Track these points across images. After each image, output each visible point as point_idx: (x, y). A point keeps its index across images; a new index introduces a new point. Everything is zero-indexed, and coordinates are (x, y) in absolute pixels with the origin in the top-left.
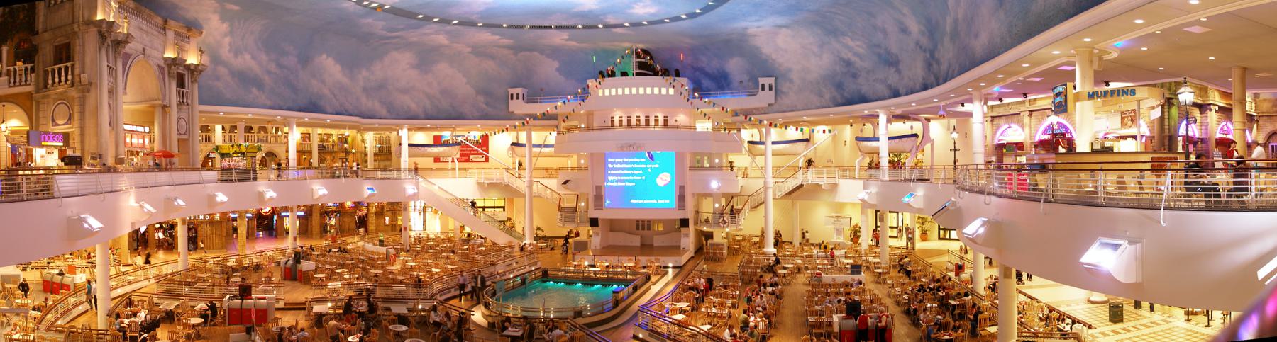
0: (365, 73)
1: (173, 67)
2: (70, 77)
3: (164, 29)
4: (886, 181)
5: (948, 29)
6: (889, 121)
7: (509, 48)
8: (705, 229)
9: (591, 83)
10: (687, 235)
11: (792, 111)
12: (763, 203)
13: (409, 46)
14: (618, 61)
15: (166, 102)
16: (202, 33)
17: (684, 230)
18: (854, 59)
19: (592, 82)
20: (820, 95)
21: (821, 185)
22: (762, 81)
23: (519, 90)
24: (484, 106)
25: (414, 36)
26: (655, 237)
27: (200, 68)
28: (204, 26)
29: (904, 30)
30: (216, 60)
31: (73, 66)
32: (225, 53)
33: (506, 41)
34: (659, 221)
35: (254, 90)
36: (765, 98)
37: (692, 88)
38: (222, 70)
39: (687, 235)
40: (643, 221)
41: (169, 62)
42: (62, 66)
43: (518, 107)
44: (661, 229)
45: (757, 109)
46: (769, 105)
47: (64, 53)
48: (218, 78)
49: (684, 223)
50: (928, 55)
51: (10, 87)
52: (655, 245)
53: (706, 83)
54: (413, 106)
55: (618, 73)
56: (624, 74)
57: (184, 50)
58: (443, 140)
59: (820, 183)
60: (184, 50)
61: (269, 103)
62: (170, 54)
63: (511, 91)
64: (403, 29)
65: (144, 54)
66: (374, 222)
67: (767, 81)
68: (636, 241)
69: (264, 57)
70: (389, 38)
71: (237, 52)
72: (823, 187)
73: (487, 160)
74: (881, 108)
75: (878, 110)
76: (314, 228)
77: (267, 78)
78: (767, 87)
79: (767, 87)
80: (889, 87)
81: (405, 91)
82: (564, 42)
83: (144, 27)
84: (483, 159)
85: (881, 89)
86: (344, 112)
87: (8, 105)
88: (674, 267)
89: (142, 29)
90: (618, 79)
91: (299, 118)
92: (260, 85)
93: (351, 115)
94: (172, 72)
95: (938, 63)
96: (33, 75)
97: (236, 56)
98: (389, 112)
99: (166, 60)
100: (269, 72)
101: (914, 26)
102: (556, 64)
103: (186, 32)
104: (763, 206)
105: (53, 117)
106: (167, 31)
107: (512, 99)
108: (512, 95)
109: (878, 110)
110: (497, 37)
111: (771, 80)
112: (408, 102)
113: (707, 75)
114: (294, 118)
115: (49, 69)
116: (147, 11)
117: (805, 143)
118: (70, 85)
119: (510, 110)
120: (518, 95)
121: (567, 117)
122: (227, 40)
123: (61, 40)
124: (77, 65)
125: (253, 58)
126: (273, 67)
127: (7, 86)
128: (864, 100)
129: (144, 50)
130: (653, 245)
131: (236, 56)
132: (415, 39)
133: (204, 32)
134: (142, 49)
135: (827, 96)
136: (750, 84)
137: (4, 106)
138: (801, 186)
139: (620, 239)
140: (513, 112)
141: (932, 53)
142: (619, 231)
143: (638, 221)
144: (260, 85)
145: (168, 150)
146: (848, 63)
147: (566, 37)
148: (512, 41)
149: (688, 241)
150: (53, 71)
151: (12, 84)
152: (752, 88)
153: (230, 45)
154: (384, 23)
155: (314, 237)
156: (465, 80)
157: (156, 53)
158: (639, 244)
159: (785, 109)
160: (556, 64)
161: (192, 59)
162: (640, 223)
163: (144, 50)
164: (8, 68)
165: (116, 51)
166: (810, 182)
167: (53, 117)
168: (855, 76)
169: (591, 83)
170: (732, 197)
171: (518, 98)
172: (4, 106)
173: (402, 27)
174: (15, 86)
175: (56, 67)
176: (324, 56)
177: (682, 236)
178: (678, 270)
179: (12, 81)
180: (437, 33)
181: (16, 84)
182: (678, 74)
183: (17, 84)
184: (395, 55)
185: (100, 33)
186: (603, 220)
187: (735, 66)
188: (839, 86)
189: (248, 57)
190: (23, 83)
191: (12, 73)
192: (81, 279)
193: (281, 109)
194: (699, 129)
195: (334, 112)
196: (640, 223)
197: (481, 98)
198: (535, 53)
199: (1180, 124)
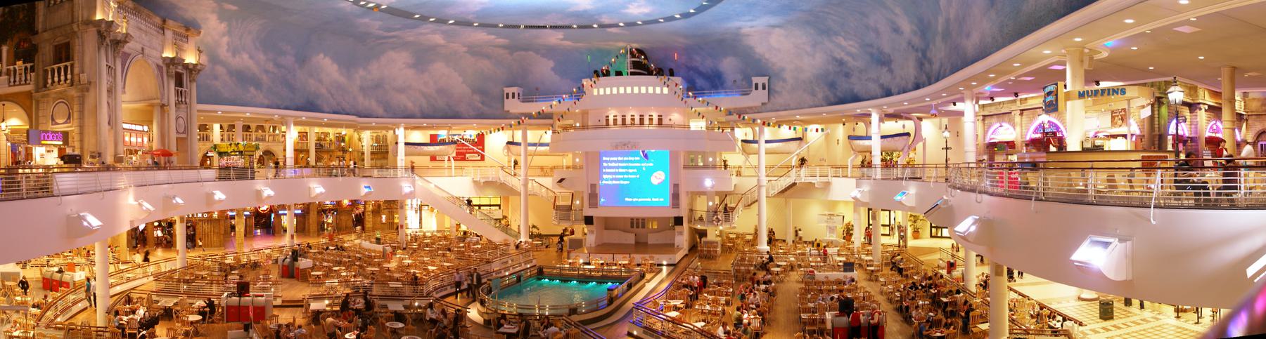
0: (361, 72)
1: (171, 67)
2: (69, 76)
3: (163, 29)
4: (879, 179)
5: (940, 29)
6: (881, 120)
7: (504, 47)
8: (699, 227)
9: (586, 82)
10: (681, 233)
11: (786, 110)
12: (757, 201)
13: (405, 45)
14: (613, 60)
15: (165, 101)
16: (200, 32)
17: (678, 228)
18: (846, 58)
19: (587, 82)
20: (813, 94)
21: (814, 184)
22: (755, 80)
23: (515, 90)
24: (480, 105)
25: (410, 36)
26: (649, 235)
27: (198, 67)
28: (202, 26)
29: (896, 30)
30: (214, 59)
31: (72, 66)
32: (223, 52)
33: (501, 41)
34: (653, 219)
35: (252, 89)
36: (758, 97)
37: (686, 87)
38: (220, 70)
39: (681, 233)
40: (638, 219)
41: (168, 61)
42: (62, 65)
43: (514, 106)
44: (655, 227)
45: (751, 108)
46: (763, 104)
47: (64, 53)
48: (216, 78)
49: (678, 221)
50: (920, 55)
51: (10, 86)
52: (649, 243)
53: (700, 82)
54: (410, 105)
55: (612, 72)
56: (619, 73)
57: (183, 50)
58: (440, 138)
59: (813, 182)
60: (183, 50)
61: (266, 102)
62: (169, 54)
63: (507, 90)
64: (399, 29)
65: (143, 54)
66: (371, 220)
67: (760, 80)
68: (630, 239)
69: (262, 57)
70: (385, 38)
71: (235, 52)
72: (816, 186)
73: (483, 158)
74: (873, 107)
75: (870, 109)
76: (311, 226)
77: (264, 78)
78: (760, 87)
79: (760, 87)
80: (882, 86)
81: (401, 90)
82: (559, 42)
83: (143, 27)
84: (479, 158)
85: (873, 88)
86: (341, 111)
87: (8, 104)
88: (668, 265)
89: (141, 29)
90: (613, 78)
91: (296, 117)
92: (257, 84)
93: (348, 114)
94: (171, 71)
95: (930, 63)
96: (33, 74)
97: (234, 55)
98: (386, 111)
99: (165, 59)
100: (267, 72)
101: (906, 26)
102: (551, 64)
103: (184, 32)
104: (756, 204)
105: (52, 115)
106: (165, 31)
107: (508, 98)
108: (508, 94)
109: (870, 109)
110: (493, 37)
111: (765, 80)
112: (404, 101)
113: (701, 74)
114: (292, 117)
115: (49, 68)
116: (146, 11)
117: (798, 142)
118: (70, 85)
119: (506, 109)
120: (513, 94)
121: (562, 116)
122: (225, 39)
123: (61, 40)
124: (76, 65)
125: (251, 57)
126: (270, 66)
127: (7, 85)
128: (856, 99)
129: (143, 49)
130: (647, 243)
131: (234, 55)
132: (411, 39)
133: (203, 32)
134: (140, 49)
135: (820, 96)
136: (744, 83)
137: (4, 105)
138: (794, 184)
139: (615, 237)
140: (508, 111)
141: (924, 52)
142: (614, 229)
143: (632, 219)
144: (257, 84)
145: (167, 148)
146: (841, 63)
147: (561, 37)
148: (507, 41)
149: (682, 239)
150: (53, 71)
151: (12, 84)
152: (746, 87)
153: (228, 44)
154: (380, 23)
155: (311, 235)
156: (461, 79)
157: (154, 53)
158: (633, 242)
159: (778, 108)
160: (551, 64)
161: (190, 58)
162: (635, 221)
163: (143, 49)
164: (8, 67)
165: (115, 51)
166: (803, 181)
167: (52, 115)
168: (847, 75)
169: (586, 82)
170: (726, 196)
171: (513, 97)
172: (4, 105)
173: (398, 26)
174: (14, 85)
175: (55, 66)
176: (322, 56)
177: (676, 234)
178: (672, 268)
179: (12, 80)
180: (434, 32)
181: (16, 83)
182: (672, 73)
183: (16, 83)
184: (392, 54)
185: (99, 32)
186: (598, 218)
187: (728, 66)
188: (832, 85)
189: (246, 56)
190: (23, 82)
191: (12, 72)
192: (80, 276)
193: (279, 108)
194: (693, 128)
195: (331, 111)
196: (635, 221)
197: (477, 98)
198: (531, 53)
199: (1170, 123)
